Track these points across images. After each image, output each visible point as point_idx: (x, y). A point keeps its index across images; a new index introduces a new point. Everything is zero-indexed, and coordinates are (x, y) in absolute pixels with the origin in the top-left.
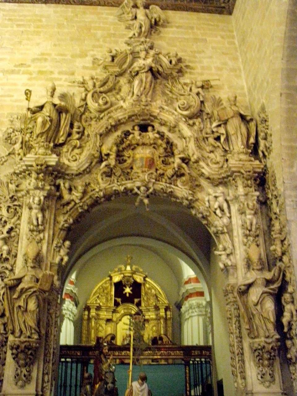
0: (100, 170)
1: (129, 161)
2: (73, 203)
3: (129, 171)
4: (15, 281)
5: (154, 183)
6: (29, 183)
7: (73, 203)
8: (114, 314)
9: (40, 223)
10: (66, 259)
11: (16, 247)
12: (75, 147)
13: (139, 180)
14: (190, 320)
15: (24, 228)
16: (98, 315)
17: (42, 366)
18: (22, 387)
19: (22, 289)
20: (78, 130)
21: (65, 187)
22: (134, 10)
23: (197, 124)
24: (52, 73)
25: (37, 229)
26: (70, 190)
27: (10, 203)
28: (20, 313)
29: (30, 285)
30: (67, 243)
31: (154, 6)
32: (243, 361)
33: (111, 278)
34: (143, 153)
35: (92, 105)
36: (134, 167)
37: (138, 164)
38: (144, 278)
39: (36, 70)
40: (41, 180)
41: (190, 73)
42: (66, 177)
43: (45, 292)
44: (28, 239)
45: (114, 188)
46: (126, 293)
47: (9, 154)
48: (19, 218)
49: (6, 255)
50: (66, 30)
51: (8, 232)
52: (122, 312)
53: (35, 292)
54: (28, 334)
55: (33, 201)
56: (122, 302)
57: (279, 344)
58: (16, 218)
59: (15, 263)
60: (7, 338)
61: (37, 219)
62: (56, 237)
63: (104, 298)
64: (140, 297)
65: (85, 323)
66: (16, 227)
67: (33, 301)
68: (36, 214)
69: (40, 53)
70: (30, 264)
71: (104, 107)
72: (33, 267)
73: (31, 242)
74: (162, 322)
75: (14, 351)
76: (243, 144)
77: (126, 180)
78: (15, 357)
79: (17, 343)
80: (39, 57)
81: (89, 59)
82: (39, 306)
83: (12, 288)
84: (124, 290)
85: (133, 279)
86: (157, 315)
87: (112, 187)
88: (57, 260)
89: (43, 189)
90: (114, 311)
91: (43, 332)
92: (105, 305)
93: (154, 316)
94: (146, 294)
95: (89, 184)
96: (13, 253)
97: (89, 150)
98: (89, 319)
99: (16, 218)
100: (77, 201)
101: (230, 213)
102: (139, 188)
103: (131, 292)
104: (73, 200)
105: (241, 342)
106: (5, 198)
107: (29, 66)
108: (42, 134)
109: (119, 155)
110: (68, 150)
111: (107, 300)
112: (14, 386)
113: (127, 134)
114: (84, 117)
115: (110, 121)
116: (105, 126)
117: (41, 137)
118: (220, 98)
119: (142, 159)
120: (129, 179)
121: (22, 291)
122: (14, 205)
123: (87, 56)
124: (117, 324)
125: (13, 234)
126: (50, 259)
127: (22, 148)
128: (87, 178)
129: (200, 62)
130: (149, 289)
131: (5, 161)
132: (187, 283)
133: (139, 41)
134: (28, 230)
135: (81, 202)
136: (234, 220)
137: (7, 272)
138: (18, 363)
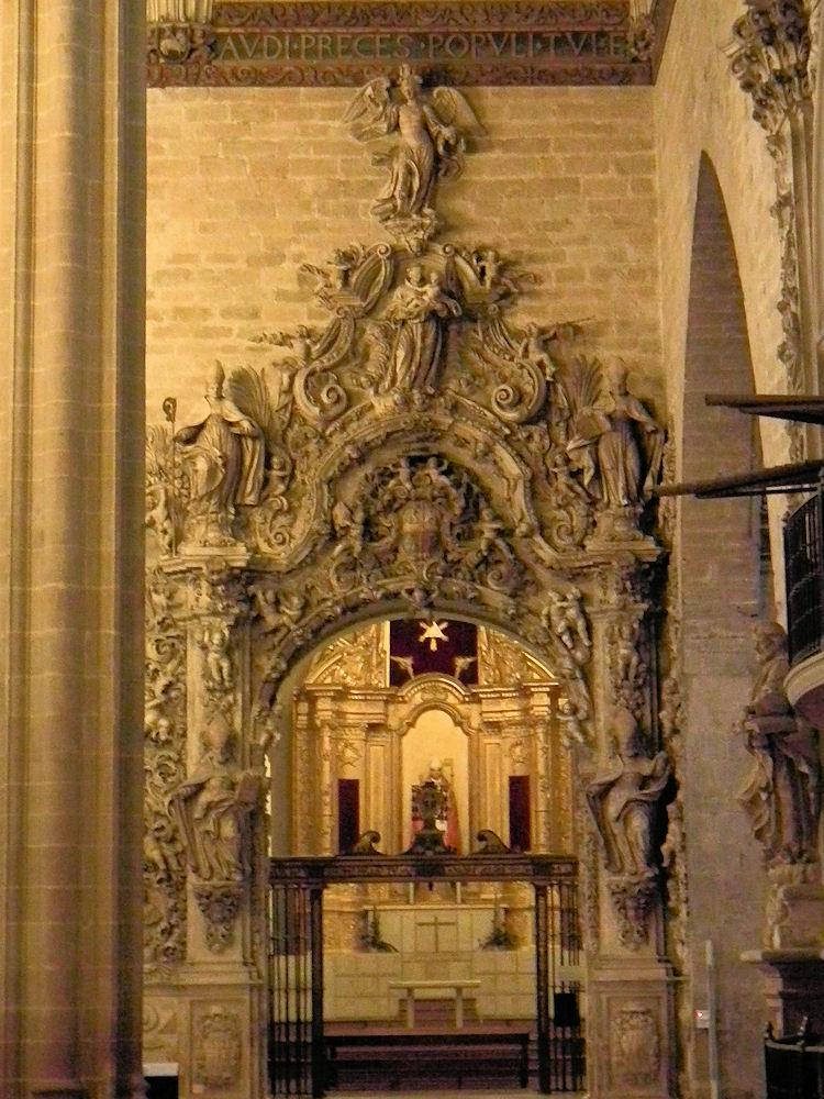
0: (334, 560)
1: (389, 539)
2: (284, 631)
3: (391, 557)
5: (441, 582)
7: (284, 631)
8: (391, 708)
12: (279, 512)
15: (194, 682)
16: (340, 714)
21: (266, 601)
22: (391, 109)
23: (536, 437)
24: (205, 312)
29: (223, 796)
37: (407, 545)
40: (220, 598)
41: (533, 294)
44: (206, 706)
45: (362, 596)
46: (428, 640)
48: (182, 662)
50: (225, 178)
51: (164, 692)
52: (418, 699)
54: (225, 873)
55: (210, 640)
56: (417, 670)
57: (652, 885)
59: (183, 747)
60: (185, 878)
61: (220, 670)
62: (257, 696)
63: (359, 658)
64: (474, 653)
65: (301, 740)
66: (178, 680)
67: (231, 823)
68: (217, 660)
69: (171, 256)
70: (216, 753)
74: (541, 736)
75: (204, 901)
76: (628, 495)
77: (386, 577)
78: (206, 910)
80: (172, 267)
84: (423, 631)
87: (357, 594)
90: (391, 700)
92: (362, 683)
93: (517, 716)
95: (313, 587)
97: (303, 526)
98: (313, 730)
102: (410, 592)
103: (445, 638)
104: (284, 625)
108: (209, 495)
109: (370, 531)
110: (265, 518)
113: (386, 474)
114: (291, 434)
116: (337, 462)
118: (596, 360)
119: (414, 535)
120: (391, 576)
123: (283, 257)
125: (173, 694)
126: (250, 738)
128: (309, 577)
137: (171, 764)
138: (209, 917)
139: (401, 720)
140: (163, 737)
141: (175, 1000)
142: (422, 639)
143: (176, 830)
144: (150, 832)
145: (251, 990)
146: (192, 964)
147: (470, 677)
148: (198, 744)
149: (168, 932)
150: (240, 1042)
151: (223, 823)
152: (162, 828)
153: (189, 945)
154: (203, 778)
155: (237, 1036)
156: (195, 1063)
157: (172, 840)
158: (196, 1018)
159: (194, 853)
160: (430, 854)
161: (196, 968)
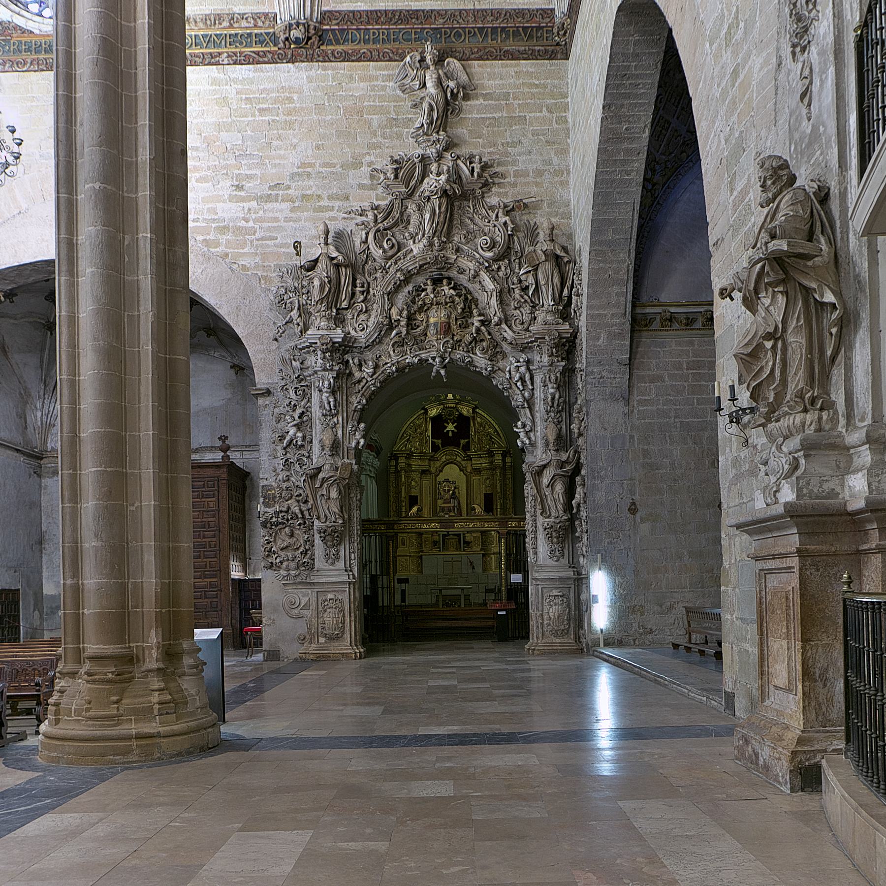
2: (364, 381)
3: (423, 338)
6: (315, 361)
7: (364, 381)
8: (432, 463)
13: (433, 351)
15: (316, 412)
20: (361, 289)
25: (329, 414)
26: (360, 365)
30: (362, 425)
31: (450, 59)
32: (536, 538)
33: (426, 413)
34: (436, 317)
35: (377, 253)
36: (428, 334)
37: (432, 331)
38: (474, 412)
39: (299, 193)
42: (355, 350)
43: (344, 479)
45: (407, 361)
46: (448, 431)
47: (286, 323)
54: (333, 519)
58: (305, 400)
61: (329, 403)
65: (392, 478)
71: (390, 253)
72: (332, 455)
75: (322, 535)
76: (554, 299)
78: (324, 540)
79: (324, 527)
81: (366, 169)
82: (340, 493)
86: (491, 463)
89: (332, 370)
91: (346, 517)
96: (308, 438)
98: (397, 472)
99: (305, 400)
100: (369, 379)
101: (532, 384)
102: (434, 359)
105: (535, 520)
107: (289, 187)
109: (410, 318)
111: (421, 445)
113: (419, 290)
114: (367, 267)
115: (398, 275)
117: (321, 304)
119: (435, 324)
121: (323, 481)
125: (305, 419)
126: (346, 443)
127: (300, 316)
128: (377, 351)
129: (515, 162)
130: (481, 424)
131: (283, 332)
133: (429, 141)
136: (537, 393)
137: (305, 459)
149: (305, 553)
152: (300, 495)
155: (343, 611)
160: (447, 516)
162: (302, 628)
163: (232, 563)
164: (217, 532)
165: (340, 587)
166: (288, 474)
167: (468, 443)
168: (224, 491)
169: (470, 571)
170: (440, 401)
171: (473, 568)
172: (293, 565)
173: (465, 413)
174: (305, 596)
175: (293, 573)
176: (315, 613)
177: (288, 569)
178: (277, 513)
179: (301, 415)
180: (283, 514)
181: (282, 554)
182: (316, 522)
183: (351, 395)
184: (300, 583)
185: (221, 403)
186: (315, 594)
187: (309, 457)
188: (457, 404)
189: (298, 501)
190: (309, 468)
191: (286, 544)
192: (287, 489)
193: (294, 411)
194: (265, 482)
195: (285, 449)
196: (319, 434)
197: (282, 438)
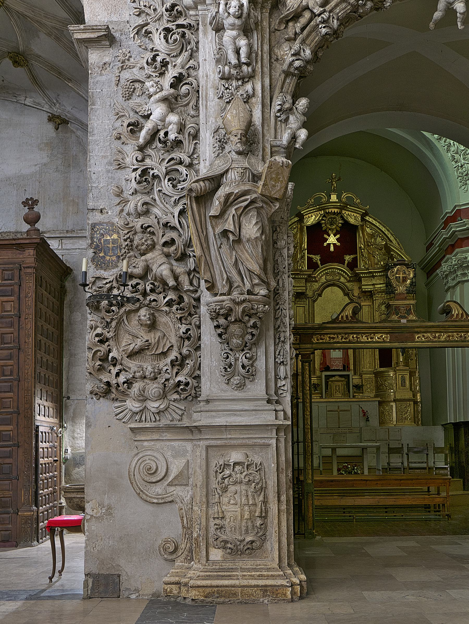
2: (307, 15)
4: (207, 183)
7: (307, 15)
8: (308, 284)
9: (243, 60)
10: (303, 134)
11: (193, 117)
14: (458, 289)
15: (208, 73)
17: (272, 348)
18: (241, 386)
19: (228, 196)
25: (236, 75)
27: (168, 21)
28: (225, 248)
33: (301, 218)
38: (363, 219)
46: (329, 244)
49: (177, 135)
52: (323, 279)
53: (253, 202)
54: (248, 285)
55: (226, 10)
56: (323, 262)
58: (185, 54)
60: (198, 300)
61: (237, 51)
62: (277, 90)
70: (234, 144)
73: (228, 103)
75: (222, 321)
78: (223, 334)
79: (228, 304)
83: (203, 198)
85: (342, 217)
88: (285, 138)
90: (309, 279)
94: (367, 245)
99: (185, 54)
100: (317, 10)
103: (338, 244)
104: (307, 8)
106: (155, 10)
112: (224, 386)
122: (179, 26)
124: (314, 301)
125: (184, 89)
126: (270, 137)
130: (372, 236)
132: (453, 218)
134: (217, 76)
135: (325, 11)
137: (182, 169)
139: (314, 291)
140: (172, 136)
141: (189, 446)
142: (325, 244)
143: (189, 244)
144: (158, 247)
145: (278, 431)
146: (208, 401)
147: (353, 265)
148: (212, 141)
149: (179, 364)
150: (265, 497)
151: (244, 221)
152: (172, 242)
153: (203, 379)
154: (217, 171)
155: (263, 489)
156: (212, 523)
157: (183, 257)
158: (213, 468)
159: (209, 265)
160: (404, 321)
161: (210, 406)
162: (170, 527)
163: (38, 401)
164: (15, 351)
165: (257, 437)
166: (147, 199)
167: (355, 260)
168: (29, 285)
169: (362, 424)
170: (320, 205)
171: (367, 420)
172: (153, 388)
173: (352, 221)
174: (177, 456)
175: (153, 405)
176: (200, 495)
177: (143, 398)
178: (124, 279)
179: (178, 81)
180: (134, 282)
181: (133, 365)
182: (206, 296)
183: (279, 45)
184: (168, 428)
185: (33, 169)
186: (201, 452)
187: (190, 166)
188: (342, 208)
189: (168, 256)
190: (190, 180)
191: (139, 343)
192: (144, 229)
193: (162, 74)
194: (97, 217)
195: (141, 149)
196: (213, 114)
197: (134, 128)
